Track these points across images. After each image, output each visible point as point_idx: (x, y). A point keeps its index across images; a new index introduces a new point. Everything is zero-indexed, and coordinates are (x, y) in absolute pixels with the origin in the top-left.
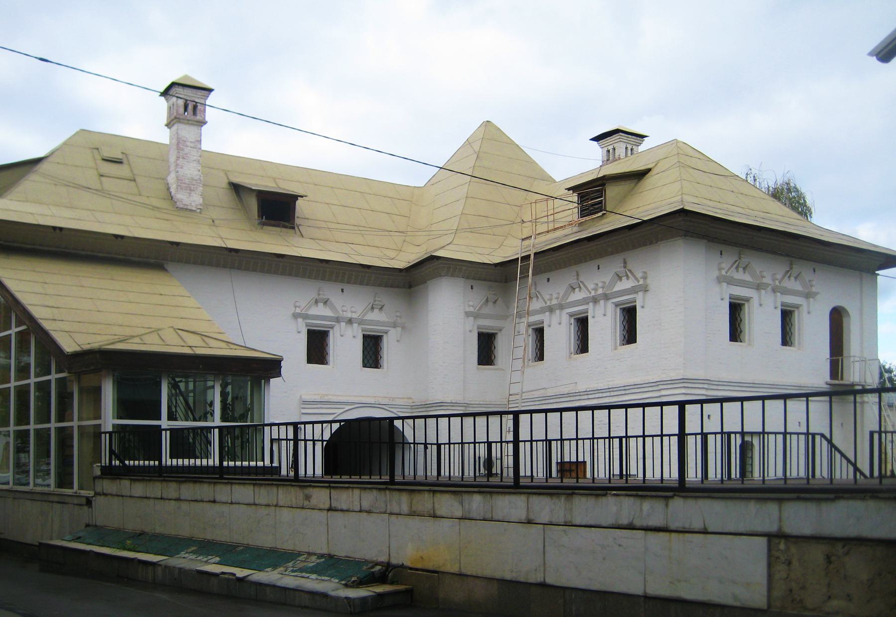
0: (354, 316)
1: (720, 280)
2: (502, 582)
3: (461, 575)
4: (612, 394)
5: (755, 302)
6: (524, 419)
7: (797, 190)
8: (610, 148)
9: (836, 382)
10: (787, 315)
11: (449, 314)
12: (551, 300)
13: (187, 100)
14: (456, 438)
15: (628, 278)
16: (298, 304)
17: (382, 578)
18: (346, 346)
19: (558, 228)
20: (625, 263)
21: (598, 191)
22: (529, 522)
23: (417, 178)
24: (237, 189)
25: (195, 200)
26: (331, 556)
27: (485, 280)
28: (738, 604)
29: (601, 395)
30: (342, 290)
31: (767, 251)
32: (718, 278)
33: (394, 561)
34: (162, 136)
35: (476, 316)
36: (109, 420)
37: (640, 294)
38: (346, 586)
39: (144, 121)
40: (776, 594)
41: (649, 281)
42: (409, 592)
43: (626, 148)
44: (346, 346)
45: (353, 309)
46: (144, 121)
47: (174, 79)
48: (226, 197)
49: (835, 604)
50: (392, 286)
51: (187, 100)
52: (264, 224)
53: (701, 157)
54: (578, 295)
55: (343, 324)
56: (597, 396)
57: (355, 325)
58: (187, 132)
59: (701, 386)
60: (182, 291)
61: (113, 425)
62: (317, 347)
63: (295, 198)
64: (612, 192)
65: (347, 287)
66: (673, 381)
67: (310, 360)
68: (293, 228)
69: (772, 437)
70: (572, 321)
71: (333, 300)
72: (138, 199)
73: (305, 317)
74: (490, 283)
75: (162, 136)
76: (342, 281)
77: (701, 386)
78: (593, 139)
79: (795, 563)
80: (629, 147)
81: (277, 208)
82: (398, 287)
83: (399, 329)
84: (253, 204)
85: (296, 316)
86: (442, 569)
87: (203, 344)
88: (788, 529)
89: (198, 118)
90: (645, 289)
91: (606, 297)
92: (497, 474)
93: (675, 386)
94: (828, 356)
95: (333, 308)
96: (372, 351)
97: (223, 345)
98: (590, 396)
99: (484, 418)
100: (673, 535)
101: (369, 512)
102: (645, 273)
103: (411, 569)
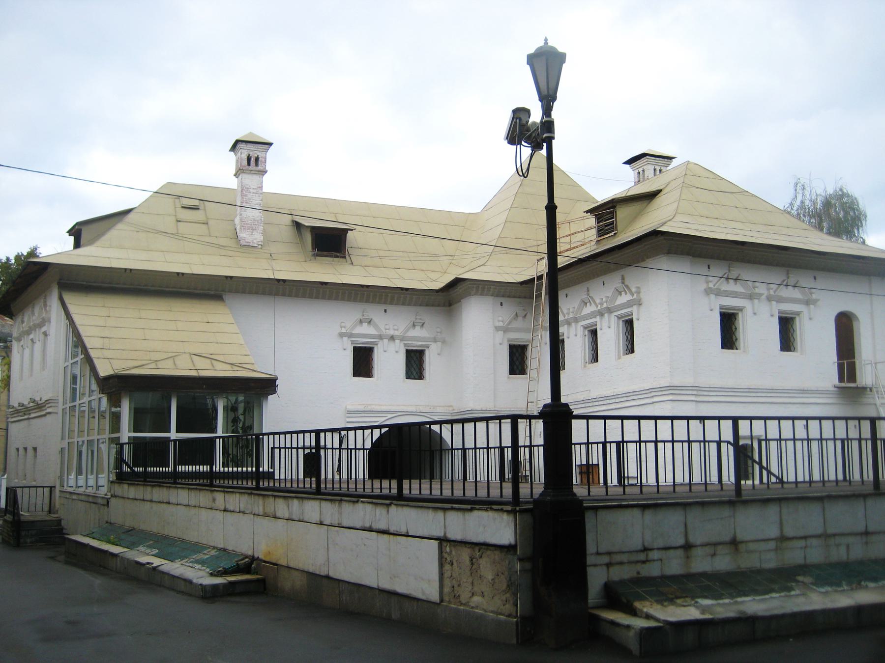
0: (396, 333)
1: (708, 292)
2: (312, 575)
3: (288, 567)
4: (617, 400)
5: (749, 310)
6: (522, 425)
7: (848, 196)
8: (640, 170)
9: (843, 385)
10: (786, 325)
11: (482, 330)
12: (568, 314)
13: (251, 153)
14: (482, 443)
15: (626, 293)
16: (343, 324)
17: (237, 570)
18: (389, 361)
19: (574, 248)
20: (623, 279)
21: (610, 213)
22: (321, 524)
23: (473, 206)
24: (298, 225)
25: (256, 238)
26: (225, 550)
27: (514, 297)
28: (424, 597)
29: (608, 402)
30: (385, 311)
31: (760, 263)
32: (705, 290)
33: (256, 556)
34: (232, 183)
35: (506, 330)
36: (126, 434)
37: (635, 307)
38: (212, 575)
39: (219, 171)
40: (447, 590)
41: (642, 295)
42: (262, 582)
43: (655, 170)
44: (389, 361)
45: (396, 327)
46: (219, 171)
47: (238, 138)
48: (288, 233)
49: (477, 599)
50: (433, 305)
51: (251, 153)
52: (317, 255)
53: (711, 175)
54: (589, 309)
55: (386, 341)
56: (605, 402)
57: (397, 341)
58: (250, 180)
59: (690, 392)
60: (230, 318)
61: (129, 438)
62: (363, 362)
63: (345, 231)
64: (622, 213)
65: (390, 308)
66: (661, 389)
67: (409, 376)
68: (345, 257)
69: (595, 446)
70: (587, 333)
71: (376, 319)
72: (207, 239)
73: (350, 335)
74: (518, 300)
75: (232, 183)
76: (385, 303)
77: (690, 392)
78: (626, 163)
79: (455, 564)
80: (658, 168)
81: (329, 241)
82: (439, 306)
83: (439, 344)
84: (308, 238)
85: (341, 335)
86: (279, 563)
87: (210, 367)
88: (452, 536)
89: (260, 168)
90: (639, 304)
91: (610, 311)
92: (526, 476)
93: (664, 393)
94: (835, 359)
95: (376, 327)
96: (415, 363)
97: (228, 367)
98: (601, 403)
99: (449, 426)
100: (392, 536)
101: (244, 513)
102: (638, 288)
103: (265, 562)
